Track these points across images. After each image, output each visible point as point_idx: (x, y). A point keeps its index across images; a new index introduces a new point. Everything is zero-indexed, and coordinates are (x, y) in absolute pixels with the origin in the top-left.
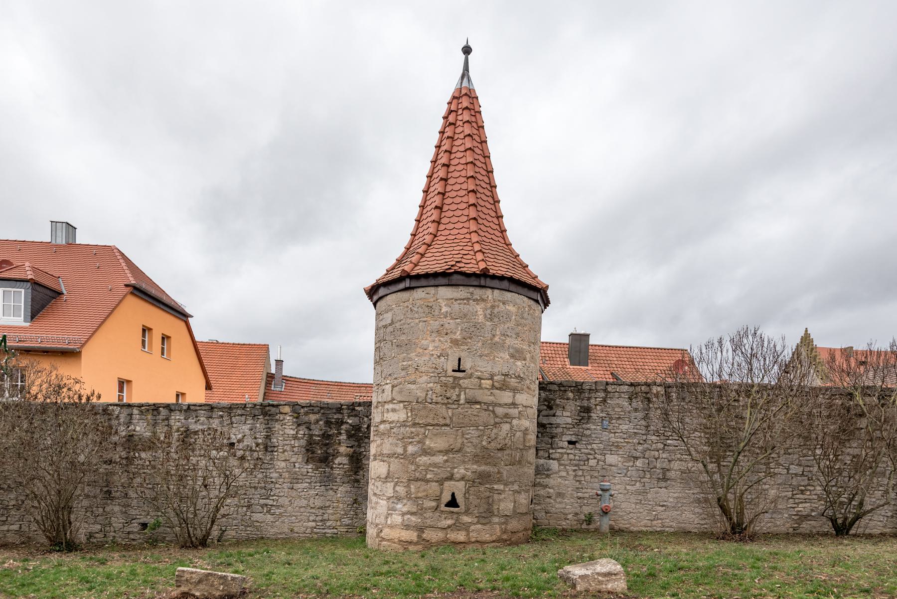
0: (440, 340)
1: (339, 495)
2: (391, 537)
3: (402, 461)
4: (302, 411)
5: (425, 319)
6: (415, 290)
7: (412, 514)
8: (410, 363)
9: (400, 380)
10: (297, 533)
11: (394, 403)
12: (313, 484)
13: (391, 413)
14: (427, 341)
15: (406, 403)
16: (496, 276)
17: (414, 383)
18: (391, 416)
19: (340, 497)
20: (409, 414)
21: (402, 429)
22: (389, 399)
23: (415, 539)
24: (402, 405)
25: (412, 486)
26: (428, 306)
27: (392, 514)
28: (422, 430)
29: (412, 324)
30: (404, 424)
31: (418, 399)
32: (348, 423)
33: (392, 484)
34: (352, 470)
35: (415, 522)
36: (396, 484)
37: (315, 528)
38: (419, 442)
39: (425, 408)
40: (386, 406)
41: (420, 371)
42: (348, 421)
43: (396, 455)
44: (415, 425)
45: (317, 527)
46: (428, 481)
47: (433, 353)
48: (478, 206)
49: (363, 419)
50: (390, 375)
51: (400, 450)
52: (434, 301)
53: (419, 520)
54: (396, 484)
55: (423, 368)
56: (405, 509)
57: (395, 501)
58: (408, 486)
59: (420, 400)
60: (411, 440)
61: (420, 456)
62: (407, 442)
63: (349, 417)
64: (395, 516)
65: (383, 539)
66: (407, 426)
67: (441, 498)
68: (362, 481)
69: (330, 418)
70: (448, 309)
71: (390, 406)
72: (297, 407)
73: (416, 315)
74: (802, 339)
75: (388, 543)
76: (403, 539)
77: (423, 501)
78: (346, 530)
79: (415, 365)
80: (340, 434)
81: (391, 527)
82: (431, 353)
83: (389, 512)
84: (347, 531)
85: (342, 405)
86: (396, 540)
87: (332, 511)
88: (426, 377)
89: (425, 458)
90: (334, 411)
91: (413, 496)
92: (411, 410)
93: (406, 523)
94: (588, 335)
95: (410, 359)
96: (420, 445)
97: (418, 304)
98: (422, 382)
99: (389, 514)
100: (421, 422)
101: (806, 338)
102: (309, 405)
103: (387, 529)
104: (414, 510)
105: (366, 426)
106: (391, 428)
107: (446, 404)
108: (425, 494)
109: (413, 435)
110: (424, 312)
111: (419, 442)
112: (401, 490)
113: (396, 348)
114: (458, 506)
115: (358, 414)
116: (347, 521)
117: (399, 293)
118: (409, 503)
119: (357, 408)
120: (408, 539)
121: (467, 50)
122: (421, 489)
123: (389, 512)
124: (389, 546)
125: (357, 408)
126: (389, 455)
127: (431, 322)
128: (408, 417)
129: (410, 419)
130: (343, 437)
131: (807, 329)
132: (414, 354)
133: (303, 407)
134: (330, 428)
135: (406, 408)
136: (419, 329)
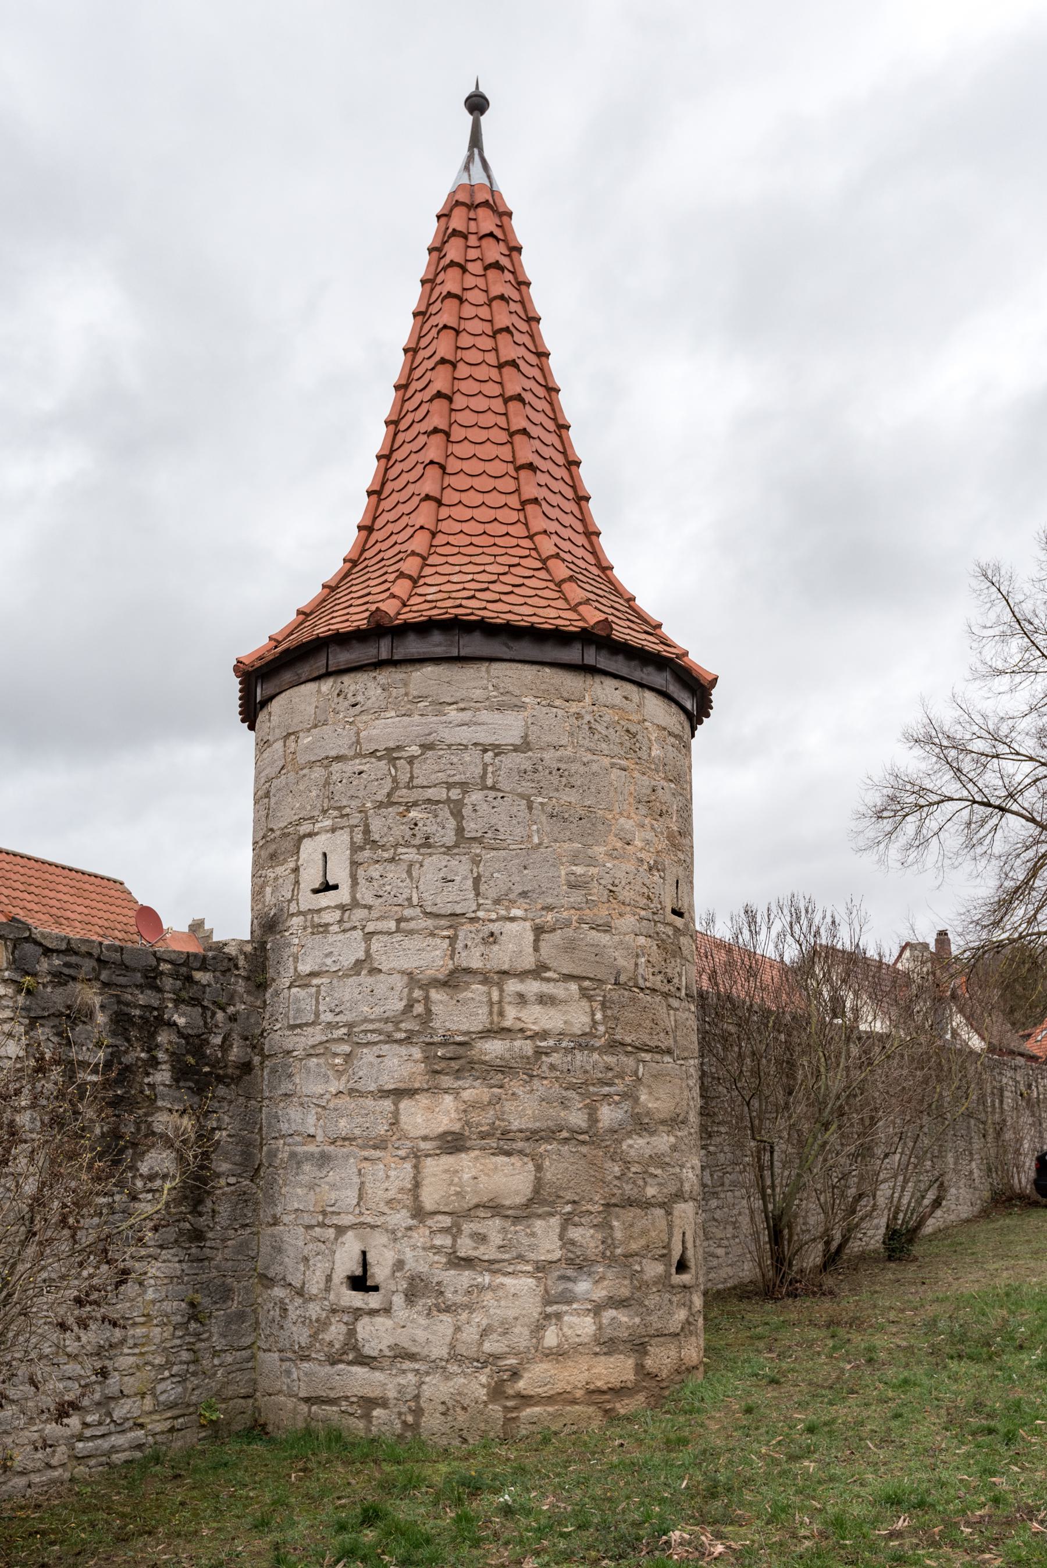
0: (653, 828)
1: (150, 1295)
2: (559, 1387)
3: (584, 1149)
4: (44, 965)
5: (624, 763)
6: (598, 679)
7: (620, 1303)
8: (593, 871)
9: (565, 914)
10: (23, 1473)
11: (548, 980)
13: (536, 1010)
14: (631, 822)
15: (587, 983)
16: (322, 638)
17: (606, 928)
18: (537, 1018)
19: (153, 1302)
20: (599, 1016)
21: (579, 1057)
22: (528, 961)
23: (630, 1376)
24: (574, 987)
25: (615, 1223)
26: (628, 731)
27: (558, 1316)
28: (630, 1062)
29: (595, 767)
30: (583, 1043)
31: (618, 974)
32: (175, 1024)
33: (555, 1221)
34: (186, 1197)
35: (628, 1328)
36: (567, 1221)
37: (81, 1438)
38: (624, 1096)
39: (633, 999)
40: (513, 986)
41: (621, 898)
42: (176, 1017)
43: (565, 1134)
44: (614, 1046)
45: (88, 1433)
46: (646, 1205)
49: (214, 1014)
50: (524, 894)
51: (577, 1118)
53: (637, 1320)
54: (567, 1221)
55: (626, 893)
56: (600, 1293)
57: (570, 1273)
58: (605, 1226)
60: (606, 1090)
61: (629, 1134)
62: (596, 1094)
63: (178, 1002)
64: (575, 1319)
65: (526, 1399)
66: (593, 1049)
67: (670, 1251)
68: (210, 1235)
69: (128, 1004)
71: (532, 987)
72: (28, 947)
73: (604, 746)
75: (550, 1409)
76: (599, 1384)
77: (640, 1263)
78: (168, 1425)
79: (606, 881)
80: (154, 1062)
81: (558, 1354)
82: (639, 855)
83: (549, 1310)
84: (172, 1430)
85: (159, 960)
86: (579, 1393)
87: (132, 1359)
88: (632, 919)
89: (641, 1142)
90: (138, 978)
91: (619, 1251)
92: (603, 1004)
93: (609, 1332)
95: (592, 861)
96: (626, 1105)
98: (624, 929)
99: (547, 1317)
102: (64, 947)
103: (545, 1366)
104: (625, 1292)
105: (217, 1040)
106: (539, 1053)
107: (666, 995)
108: (642, 1242)
109: (610, 1074)
111: (624, 1096)
112: (584, 1235)
113: (544, 818)
114: (677, 1273)
115: (198, 995)
116: (169, 1391)
117: (547, 670)
118: (610, 1275)
119: (198, 975)
120: (615, 1381)
121: (477, 104)
122: (636, 1230)
123: (549, 1310)
124: (554, 1416)
125: (198, 975)
126: (534, 1132)
127: (636, 774)
128: (595, 1023)
129: (602, 1029)
130: (163, 1076)
132: (602, 849)
133: (47, 952)
134: (128, 1040)
135: (590, 999)
136: (611, 784)
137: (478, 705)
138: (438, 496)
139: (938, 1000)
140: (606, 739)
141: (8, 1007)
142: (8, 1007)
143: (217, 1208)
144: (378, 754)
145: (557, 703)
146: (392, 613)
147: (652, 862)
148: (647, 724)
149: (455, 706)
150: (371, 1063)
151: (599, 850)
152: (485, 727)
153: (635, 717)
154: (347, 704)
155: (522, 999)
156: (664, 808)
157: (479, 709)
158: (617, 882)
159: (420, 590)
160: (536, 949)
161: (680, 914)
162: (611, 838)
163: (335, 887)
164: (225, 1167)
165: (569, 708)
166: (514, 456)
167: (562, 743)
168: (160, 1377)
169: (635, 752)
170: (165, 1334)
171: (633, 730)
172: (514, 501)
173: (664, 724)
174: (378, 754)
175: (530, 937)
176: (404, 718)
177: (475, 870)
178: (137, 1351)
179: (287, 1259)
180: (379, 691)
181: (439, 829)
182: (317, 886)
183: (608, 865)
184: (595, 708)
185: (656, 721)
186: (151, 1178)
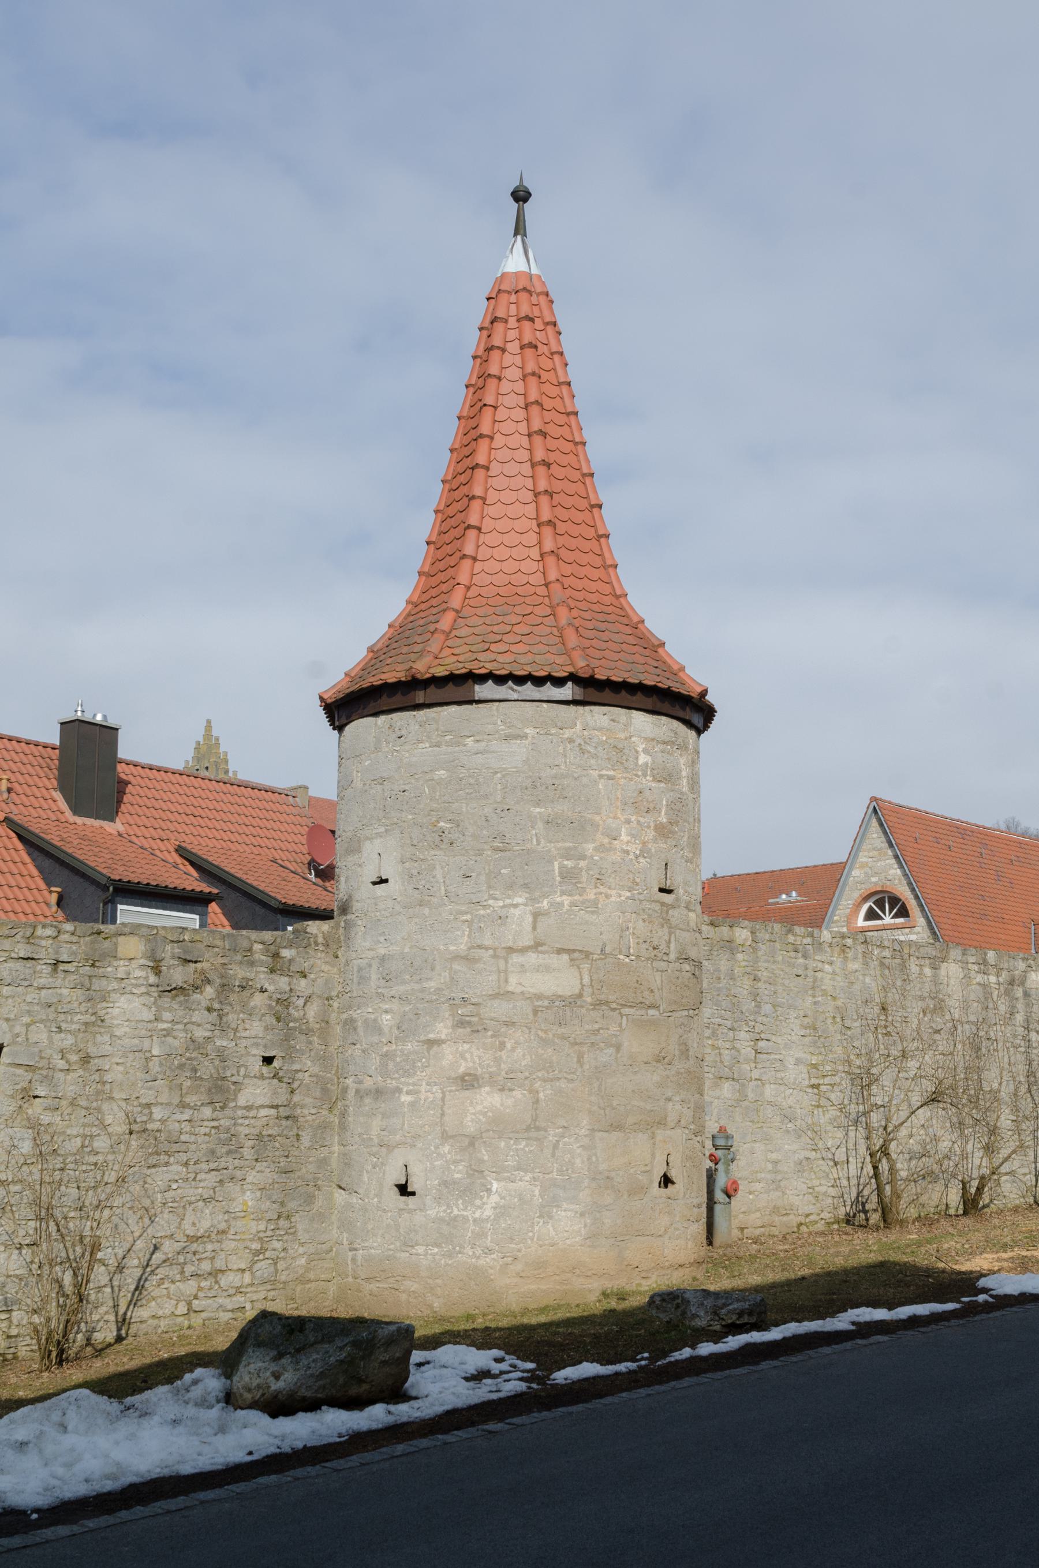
5: (611, 773)
8: (582, 864)
12: (191, 1168)
22: (527, 941)
24: (565, 957)
29: (584, 780)
31: (604, 945)
40: (516, 958)
47: (629, 848)
48: (559, 524)
52: (626, 739)
59: (608, 950)
70: (648, 759)
71: (532, 958)
73: (593, 762)
74: (197, 748)
82: (625, 848)
94: (117, 729)
97: (595, 740)
100: (612, 998)
101: (209, 747)
110: (609, 759)
121: (521, 196)
131: (209, 722)
137: (490, 737)
138: (474, 555)
139: (910, 956)
140: (595, 756)
141: (143, 985)
142: (143, 985)
143: (300, 1133)
144: (417, 776)
145: (553, 731)
146: (423, 670)
147: (638, 852)
148: (633, 739)
149: (472, 738)
150: (411, 1020)
151: (589, 848)
152: (495, 755)
153: (622, 736)
154: (395, 736)
155: (523, 969)
156: (651, 806)
157: (489, 740)
158: (603, 872)
159: (449, 643)
160: (534, 928)
161: (669, 891)
162: (599, 836)
163: (386, 881)
164: (308, 1100)
165: (563, 734)
166: (537, 516)
167: (556, 763)
168: (256, 1258)
169: (623, 763)
170: (259, 1227)
171: (620, 746)
172: (535, 553)
173: (651, 736)
174: (417, 776)
175: (529, 919)
176: (435, 748)
177: (487, 868)
178: (237, 1237)
179: (353, 1173)
180: (417, 727)
181: (460, 836)
182: (375, 879)
183: (596, 858)
184: (585, 732)
185: (643, 735)
186: (248, 1108)
